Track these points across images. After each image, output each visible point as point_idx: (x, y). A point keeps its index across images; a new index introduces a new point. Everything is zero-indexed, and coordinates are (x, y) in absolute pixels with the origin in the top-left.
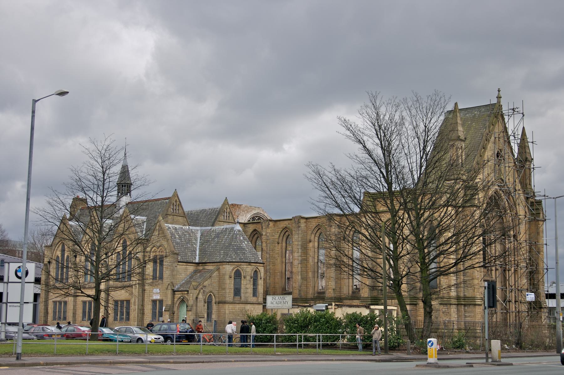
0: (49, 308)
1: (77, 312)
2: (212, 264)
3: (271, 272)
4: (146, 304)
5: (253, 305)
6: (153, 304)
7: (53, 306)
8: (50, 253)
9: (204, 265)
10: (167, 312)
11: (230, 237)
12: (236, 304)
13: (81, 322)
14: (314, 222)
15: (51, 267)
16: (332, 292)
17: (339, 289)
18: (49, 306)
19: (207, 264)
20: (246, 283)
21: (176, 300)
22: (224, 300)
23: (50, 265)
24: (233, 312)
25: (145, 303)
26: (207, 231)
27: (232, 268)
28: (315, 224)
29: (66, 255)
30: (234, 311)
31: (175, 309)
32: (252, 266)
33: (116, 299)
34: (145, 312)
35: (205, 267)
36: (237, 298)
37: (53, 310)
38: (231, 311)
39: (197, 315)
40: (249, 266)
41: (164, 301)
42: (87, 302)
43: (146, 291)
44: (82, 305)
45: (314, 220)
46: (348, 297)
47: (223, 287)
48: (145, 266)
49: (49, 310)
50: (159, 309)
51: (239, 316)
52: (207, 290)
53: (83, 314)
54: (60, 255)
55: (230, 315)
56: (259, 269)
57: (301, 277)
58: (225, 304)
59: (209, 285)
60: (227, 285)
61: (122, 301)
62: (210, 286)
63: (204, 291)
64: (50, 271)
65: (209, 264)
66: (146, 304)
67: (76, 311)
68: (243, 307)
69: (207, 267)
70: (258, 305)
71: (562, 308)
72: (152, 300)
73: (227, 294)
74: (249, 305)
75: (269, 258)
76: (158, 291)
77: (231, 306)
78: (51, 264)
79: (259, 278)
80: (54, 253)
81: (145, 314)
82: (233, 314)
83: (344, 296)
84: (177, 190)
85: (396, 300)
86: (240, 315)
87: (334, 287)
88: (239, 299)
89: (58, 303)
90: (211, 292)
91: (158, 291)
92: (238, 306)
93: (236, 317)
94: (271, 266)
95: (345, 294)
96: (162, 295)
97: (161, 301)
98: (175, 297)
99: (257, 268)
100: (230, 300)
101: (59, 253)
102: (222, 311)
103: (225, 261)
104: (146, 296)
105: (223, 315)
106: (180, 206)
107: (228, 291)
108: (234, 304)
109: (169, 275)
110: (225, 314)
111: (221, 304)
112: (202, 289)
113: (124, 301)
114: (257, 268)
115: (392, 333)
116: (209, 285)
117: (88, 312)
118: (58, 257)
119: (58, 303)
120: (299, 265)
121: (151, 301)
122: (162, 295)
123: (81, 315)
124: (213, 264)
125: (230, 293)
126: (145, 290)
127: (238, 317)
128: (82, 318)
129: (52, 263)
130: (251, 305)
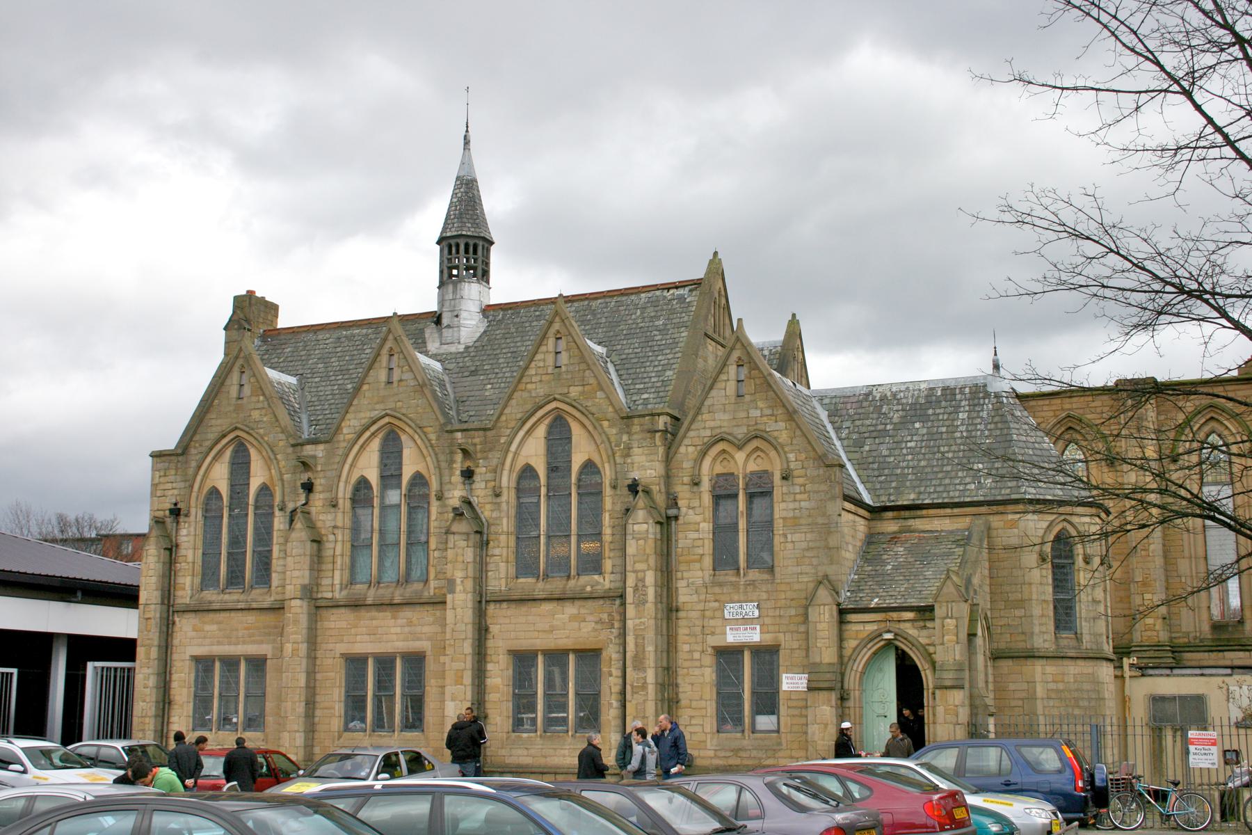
0: (174, 685)
1: (318, 698)
2: (948, 511)
4: (686, 664)
6: (718, 664)
7: (193, 676)
8: (179, 478)
9: (907, 514)
10: (823, 695)
11: (984, 414)
12: (1066, 662)
13: (340, 737)
14: (1045, 408)
15: (184, 532)
16: (1157, 627)
18: (175, 677)
19: (924, 512)
21: (851, 644)
22: (1021, 645)
23: (178, 523)
24: (1058, 691)
25: (680, 662)
26: (855, 399)
27: (1045, 525)
28: (1051, 414)
29: (255, 484)
30: (1061, 686)
31: (851, 681)
33: (525, 644)
34: (681, 696)
35: (911, 522)
36: (1067, 638)
37: (193, 689)
38: (1052, 686)
39: (978, 702)
41: (782, 653)
42: (370, 662)
43: (681, 614)
44: (343, 672)
45: (1047, 402)
46: (1201, 641)
47: (1012, 597)
48: (676, 518)
49: (172, 692)
50: (753, 682)
51: (1078, 707)
53: (346, 706)
54: (224, 489)
55: (1051, 703)
58: (1029, 662)
60: (1034, 589)
61: (385, 663)
64: (177, 546)
65: (932, 512)
66: (686, 664)
67: (314, 694)
68: (1090, 670)
69: (918, 524)
71: (961, 687)
72: (713, 647)
73: (1036, 622)
76: (751, 610)
77: (1051, 669)
78: (182, 519)
80: (199, 478)
81: (683, 702)
82: (1060, 699)
83: (1186, 640)
84: (720, 256)
86: (1081, 703)
88: (1073, 643)
89: (217, 665)
91: (751, 610)
92: (1074, 669)
93: (1070, 710)
95: (1188, 633)
96: (771, 628)
97: (766, 655)
98: (846, 635)
100: (1047, 645)
101: (220, 476)
102: (1012, 687)
103: (1013, 497)
104: (682, 631)
105: (1020, 703)
106: (726, 309)
107: (1037, 611)
108: (1060, 662)
109: (808, 549)
110: (1032, 697)
111: (1010, 662)
113: (565, 652)
117: (375, 695)
118: (215, 492)
119: (217, 665)
121: (710, 650)
122: (771, 628)
123: (339, 708)
124: (956, 511)
125: (1044, 619)
126: (677, 611)
127: (1077, 712)
128: (343, 719)
129: (187, 515)
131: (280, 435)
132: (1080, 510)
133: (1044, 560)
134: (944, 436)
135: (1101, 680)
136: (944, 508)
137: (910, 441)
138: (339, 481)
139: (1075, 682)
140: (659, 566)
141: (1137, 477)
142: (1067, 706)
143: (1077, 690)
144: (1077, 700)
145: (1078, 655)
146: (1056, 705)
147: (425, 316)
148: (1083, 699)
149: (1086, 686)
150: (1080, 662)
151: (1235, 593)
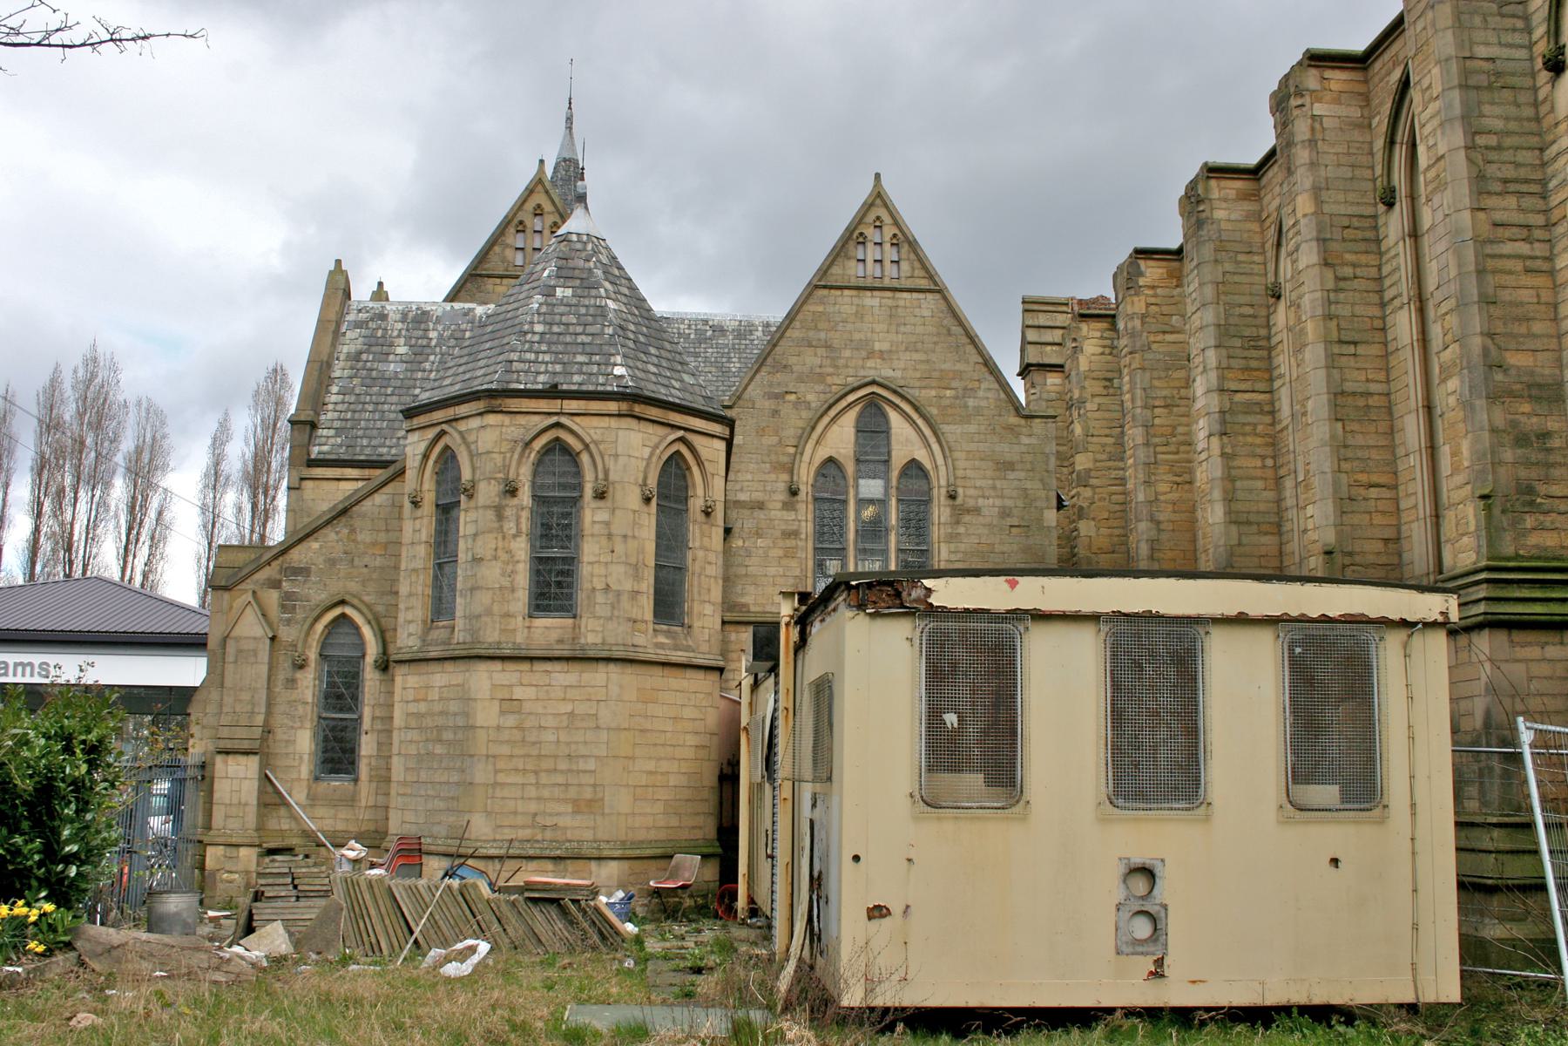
3: (1161, 517)
5: (525, 666)
17: (1380, 546)
20: (615, 529)
24: (419, 716)
30: (423, 707)
32: (522, 420)
40: (491, 419)
52: (316, 593)
56: (699, 448)
57: (1228, 513)
59: (332, 562)
62: (343, 568)
63: (288, 596)
70: (577, 667)
74: (483, 667)
75: (1147, 444)
79: (696, 504)
85: (1474, 557)
87: (1330, 537)
90: (342, 602)
94: (1163, 487)
99: (681, 440)
112: (276, 584)
114: (681, 440)
115: (733, 970)
116: (332, 562)
120: (1215, 441)
130: (511, 666)
131: (1161, 518)
132: (463, 410)
133: (647, 500)
134: (619, 359)
135: (473, 696)
136: (431, 411)
137: (544, 352)
138: (480, 414)
139: (441, 699)
140: (1484, 542)
141: (1240, 535)
142: (427, 740)
143: (442, 713)
144: (440, 729)
145: (447, 654)
146: (416, 738)
147: (1349, 574)
148: (446, 728)
149: (453, 707)
150: (449, 666)
151: (419, 564)
